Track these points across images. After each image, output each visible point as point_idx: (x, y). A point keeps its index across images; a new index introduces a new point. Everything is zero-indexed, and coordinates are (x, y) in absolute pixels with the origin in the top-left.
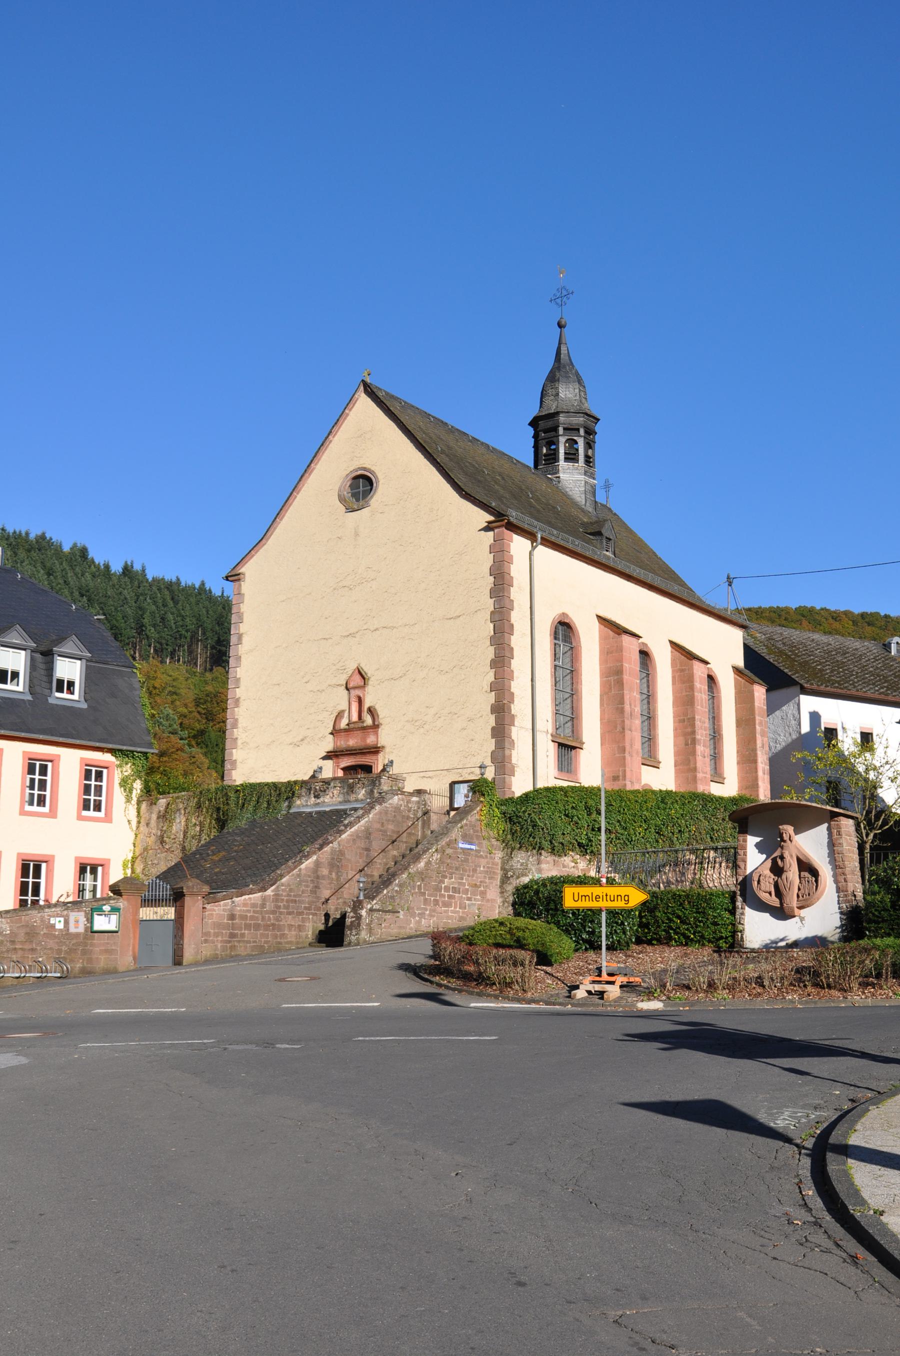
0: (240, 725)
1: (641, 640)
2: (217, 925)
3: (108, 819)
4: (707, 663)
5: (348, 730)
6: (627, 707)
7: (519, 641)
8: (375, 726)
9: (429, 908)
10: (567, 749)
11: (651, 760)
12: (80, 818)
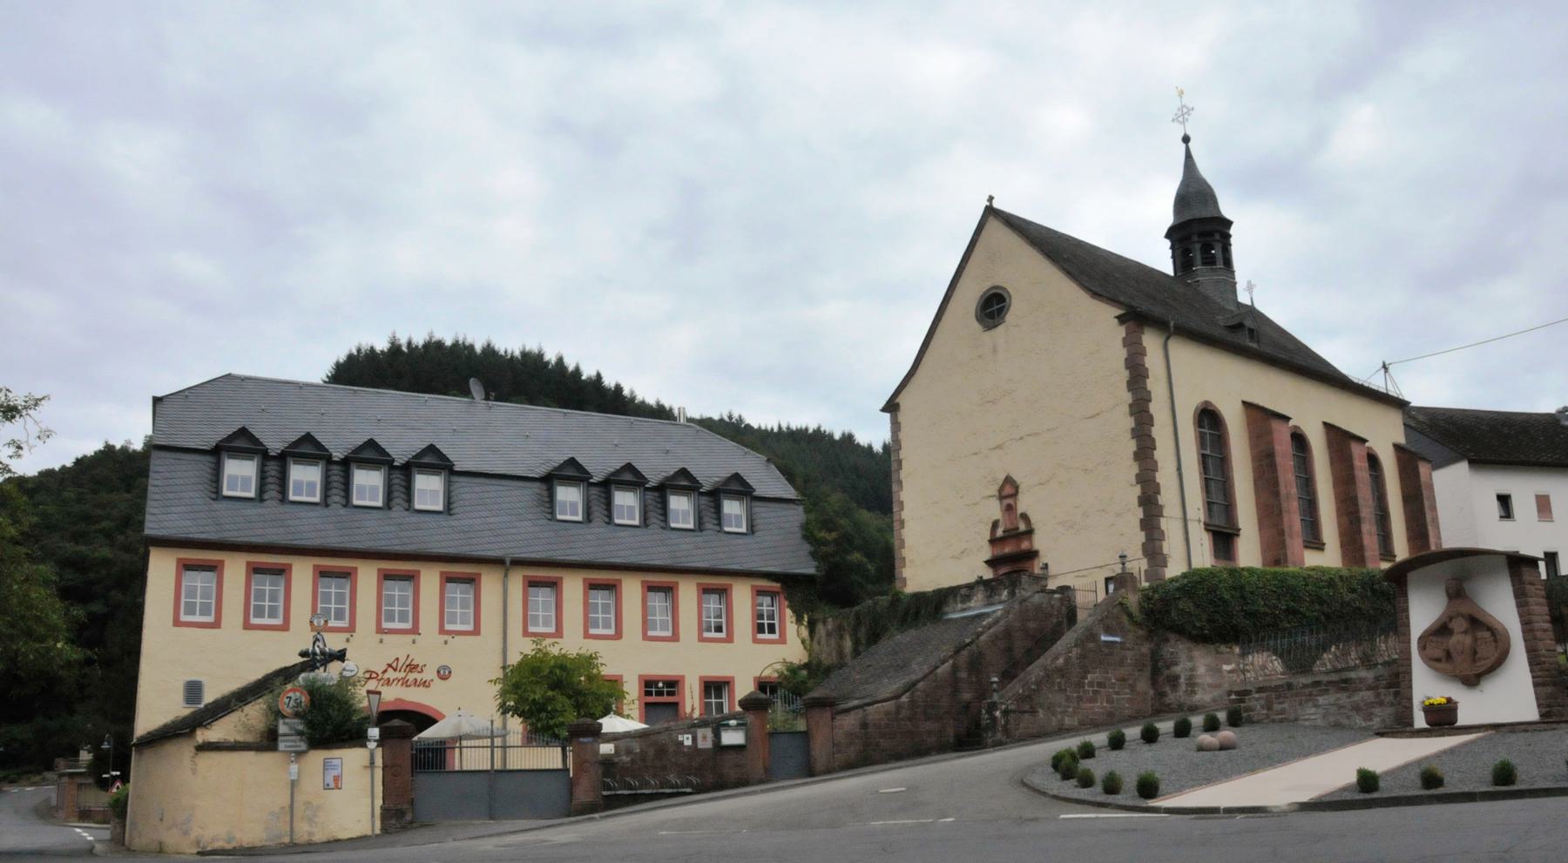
1: (1291, 423)
4: (1364, 441)
5: (1002, 540)
6: (1283, 491)
7: (1161, 432)
8: (1030, 532)
10: (1224, 538)
11: (1315, 543)
12: (755, 641)
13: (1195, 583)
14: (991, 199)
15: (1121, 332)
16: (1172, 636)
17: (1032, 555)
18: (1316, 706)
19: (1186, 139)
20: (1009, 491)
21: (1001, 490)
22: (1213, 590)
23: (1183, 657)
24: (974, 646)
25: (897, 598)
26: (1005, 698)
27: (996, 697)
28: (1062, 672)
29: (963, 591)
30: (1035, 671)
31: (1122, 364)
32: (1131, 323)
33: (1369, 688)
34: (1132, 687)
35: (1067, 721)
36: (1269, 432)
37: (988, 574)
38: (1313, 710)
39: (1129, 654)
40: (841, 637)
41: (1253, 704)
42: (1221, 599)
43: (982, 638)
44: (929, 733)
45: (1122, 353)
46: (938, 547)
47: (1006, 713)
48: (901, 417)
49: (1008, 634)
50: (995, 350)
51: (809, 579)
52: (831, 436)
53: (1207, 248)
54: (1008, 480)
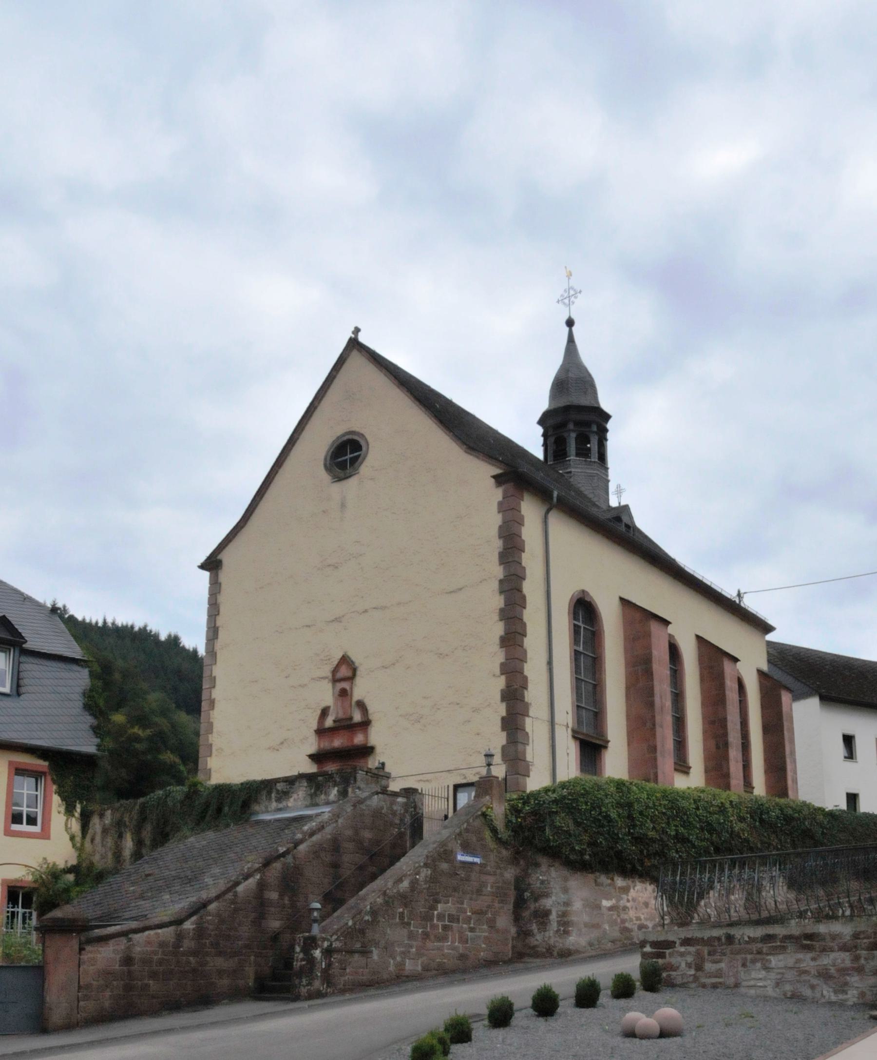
0: (215, 730)
2: (107, 974)
3: (45, 834)
5: (333, 730)
6: (657, 700)
8: (365, 724)
9: (414, 943)
10: (591, 749)
11: (683, 767)
12: (8, 833)
13: (565, 800)
14: (357, 330)
15: (498, 494)
16: (544, 861)
17: (367, 751)
18: (767, 968)
19: (570, 323)
20: (345, 672)
21: (335, 671)
22: (596, 805)
23: (555, 886)
24: (289, 859)
25: (194, 792)
26: (327, 931)
27: (316, 930)
28: (405, 899)
29: (280, 786)
30: (371, 894)
31: (494, 531)
32: (510, 486)
33: (844, 948)
34: (492, 924)
35: (409, 966)
36: (648, 635)
37: (310, 768)
38: (763, 974)
39: (491, 879)
40: (121, 836)
41: (675, 960)
42: (607, 817)
43: (302, 847)
44: (220, 973)
45: (497, 520)
46: (252, 737)
47: (328, 952)
48: (223, 576)
49: (335, 845)
50: (343, 505)
51: (85, 762)
52: (156, 636)
53: (583, 440)
54: (345, 660)
